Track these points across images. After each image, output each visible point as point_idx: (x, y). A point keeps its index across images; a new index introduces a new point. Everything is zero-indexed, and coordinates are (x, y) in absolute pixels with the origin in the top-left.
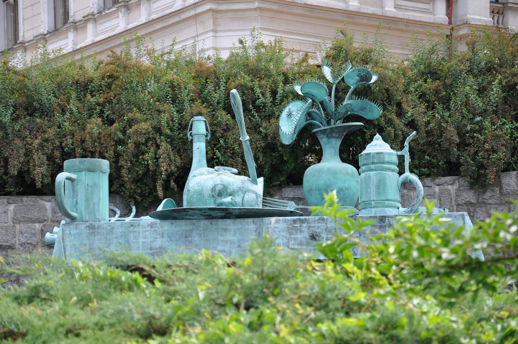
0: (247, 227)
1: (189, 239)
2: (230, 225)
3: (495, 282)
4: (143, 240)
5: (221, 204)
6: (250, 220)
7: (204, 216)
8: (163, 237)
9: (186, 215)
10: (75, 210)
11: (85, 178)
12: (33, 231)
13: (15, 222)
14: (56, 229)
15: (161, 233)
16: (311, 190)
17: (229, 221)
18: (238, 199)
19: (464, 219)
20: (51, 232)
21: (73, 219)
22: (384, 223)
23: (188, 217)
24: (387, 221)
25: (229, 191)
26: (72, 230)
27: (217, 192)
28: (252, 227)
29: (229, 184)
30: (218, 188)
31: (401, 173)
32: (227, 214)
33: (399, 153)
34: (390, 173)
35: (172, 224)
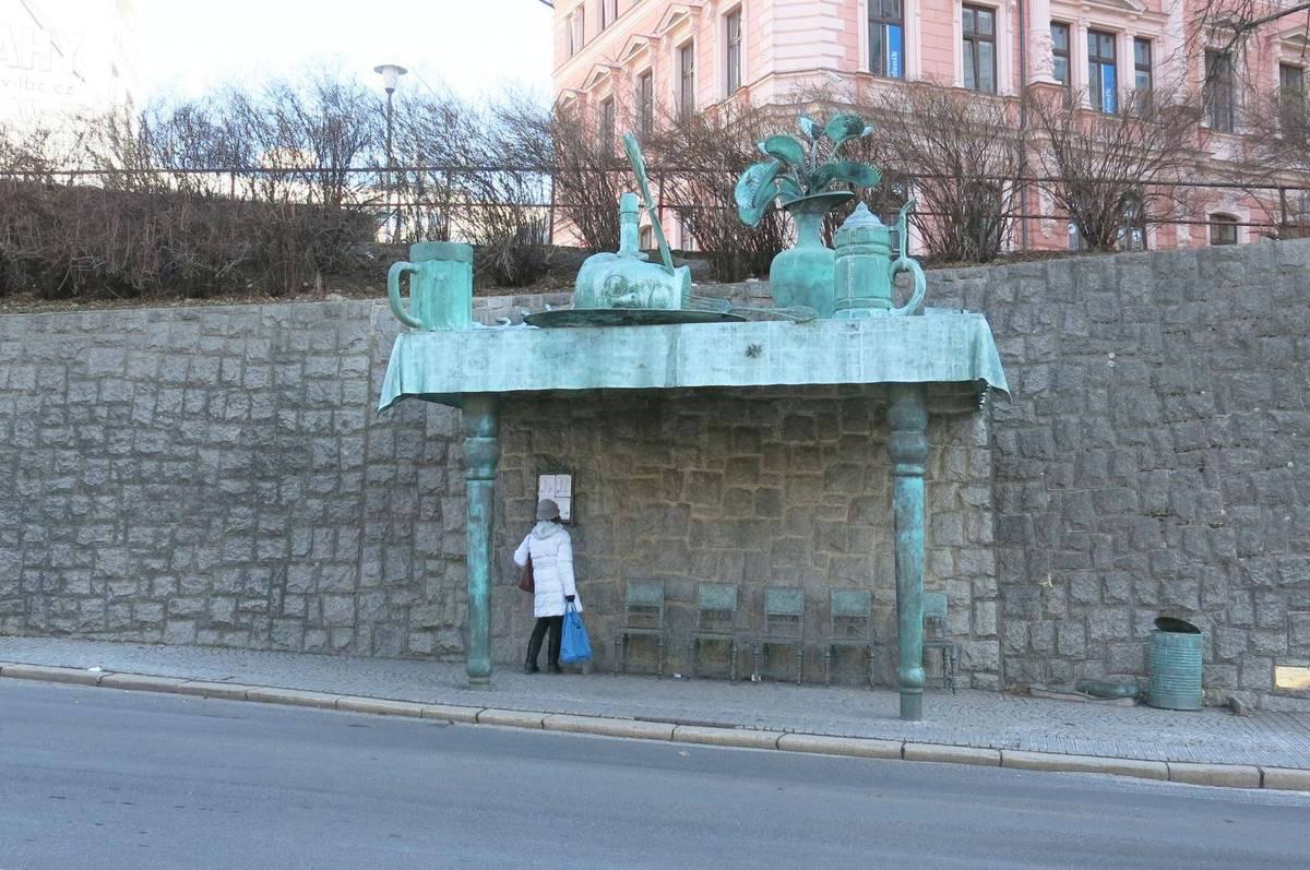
3: (1152, 595)
5: (618, 305)
17: (628, 330)
18: (643, 297)
25: (630, 285)
27: (613, 286)
31: (894, 258)
33: (892, 229)
34: (878, 257)
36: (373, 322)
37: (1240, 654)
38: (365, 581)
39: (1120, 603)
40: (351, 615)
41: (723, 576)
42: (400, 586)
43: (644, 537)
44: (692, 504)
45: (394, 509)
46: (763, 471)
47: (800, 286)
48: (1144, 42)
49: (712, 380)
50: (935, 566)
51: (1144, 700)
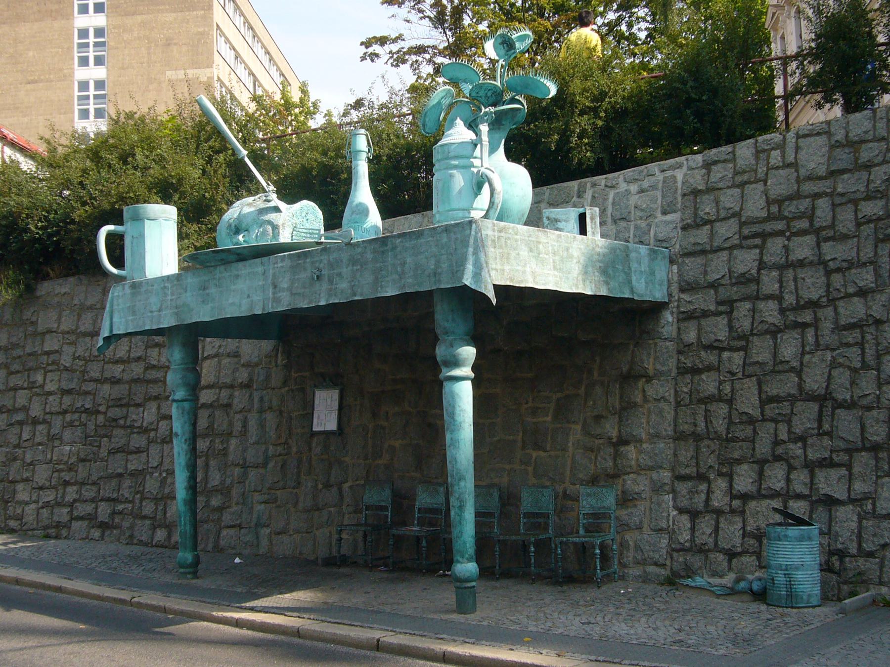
28: (260, 269)
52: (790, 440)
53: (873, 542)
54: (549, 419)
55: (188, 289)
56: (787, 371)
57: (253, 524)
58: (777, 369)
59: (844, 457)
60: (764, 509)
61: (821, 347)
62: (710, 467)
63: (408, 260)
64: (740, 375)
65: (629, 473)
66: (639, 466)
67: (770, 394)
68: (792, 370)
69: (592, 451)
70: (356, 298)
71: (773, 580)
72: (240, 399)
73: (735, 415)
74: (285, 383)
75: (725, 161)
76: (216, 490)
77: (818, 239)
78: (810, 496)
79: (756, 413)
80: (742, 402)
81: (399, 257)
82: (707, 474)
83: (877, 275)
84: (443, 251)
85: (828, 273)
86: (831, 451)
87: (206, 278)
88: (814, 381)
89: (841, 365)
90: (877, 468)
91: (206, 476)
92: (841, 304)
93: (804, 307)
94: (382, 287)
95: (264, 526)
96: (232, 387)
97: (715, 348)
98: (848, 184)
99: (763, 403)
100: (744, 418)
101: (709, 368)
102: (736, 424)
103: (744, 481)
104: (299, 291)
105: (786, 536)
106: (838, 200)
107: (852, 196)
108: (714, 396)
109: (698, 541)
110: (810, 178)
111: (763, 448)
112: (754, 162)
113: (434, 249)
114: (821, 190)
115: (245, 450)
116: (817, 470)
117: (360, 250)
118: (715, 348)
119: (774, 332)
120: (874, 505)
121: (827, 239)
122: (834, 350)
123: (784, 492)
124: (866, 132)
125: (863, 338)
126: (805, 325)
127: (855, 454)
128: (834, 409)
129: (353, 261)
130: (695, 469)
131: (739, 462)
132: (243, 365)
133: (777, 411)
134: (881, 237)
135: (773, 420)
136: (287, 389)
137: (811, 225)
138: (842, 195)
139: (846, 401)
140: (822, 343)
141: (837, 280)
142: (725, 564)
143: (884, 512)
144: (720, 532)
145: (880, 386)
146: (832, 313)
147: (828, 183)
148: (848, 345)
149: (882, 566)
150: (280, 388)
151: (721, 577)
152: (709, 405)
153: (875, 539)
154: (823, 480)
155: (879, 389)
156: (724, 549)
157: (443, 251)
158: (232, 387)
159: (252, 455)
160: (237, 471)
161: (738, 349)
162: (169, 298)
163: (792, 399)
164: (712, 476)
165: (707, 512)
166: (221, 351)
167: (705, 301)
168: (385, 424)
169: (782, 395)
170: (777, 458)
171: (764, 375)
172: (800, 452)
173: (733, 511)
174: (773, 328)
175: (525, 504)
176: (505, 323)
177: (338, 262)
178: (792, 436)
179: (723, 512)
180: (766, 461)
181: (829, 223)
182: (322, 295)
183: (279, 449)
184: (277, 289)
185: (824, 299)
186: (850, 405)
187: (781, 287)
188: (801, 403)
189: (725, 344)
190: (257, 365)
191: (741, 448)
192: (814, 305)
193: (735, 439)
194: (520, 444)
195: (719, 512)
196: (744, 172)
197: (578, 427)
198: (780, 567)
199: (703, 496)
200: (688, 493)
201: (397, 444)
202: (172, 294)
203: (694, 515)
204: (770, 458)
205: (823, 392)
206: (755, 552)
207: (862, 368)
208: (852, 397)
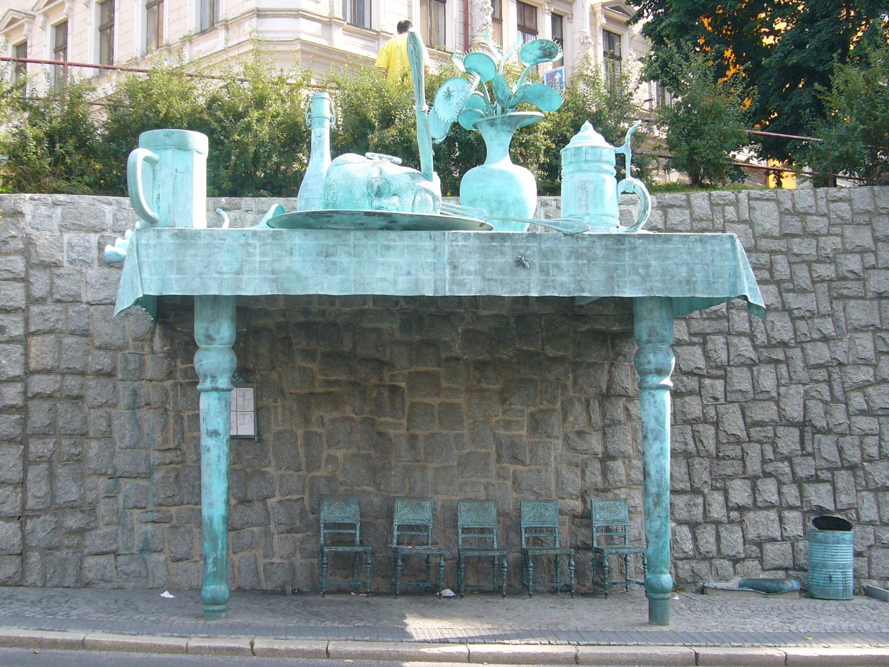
0: (421, 244)
1: (333, 259)
2: (395, 241)
4: (262, 259)
6: (425, 234)
7: (355, 225)
8: (291, 254)
9: (329, 222)
10: (156, 207)
11: (169, 157)
12: (87, 244)
13: (63, 229)
14: (119, 241)
15: (288, 249)
16: (475, 200)
17: (393, 234)
19: (733, 244)
20: (113, 245)
21: (151, 221)
22: (623, 244)
23: (330, 226)
24: (627, 242)
25: (393, 188)
26: (149, 237)
27: (375, 189)
28: (428, 244)
29: (394, 178)
30: (376, 185)
32: (391, 223)
35: (306, 235)
36: (28, 218)
37: (870, 547)
38: (31, 503)
39: (771, 506)
40: (17, 540)
41: (412, 489)
42: (73, 507)
43: (332, 452)
44: (376, 418)
45: (61, 424)
46: (444, 384)
47: (500, 203)
48: (557, 19)
49: (515, 291)
50: (610, 476)
51: (807, 592)
52: (776, 460)
53: (862, 544)
54: (524, 432)
55: (296, 252)
56: (766, 400)
57: (135, 550)
58: (757, 397)
59: (825, 475)
60: (763, 520)
61: (794, 382)
62: (705, 482)
63: (653, 263)
64: (722, 401)
65: (619, 488)
66: (630, 480)
67: (755, 419)
68: (771, 399)
69: (577, 466)
70: (584, 294)
71: (830, 577)
72: (95, 391)
73: (722, 436)
74: (170, 375)
75: (680, 207)
76: (72, 507)
77: (780, 289)
78: (802, 507)
79: (743, 434)
80: (730, 425)
81: (639, 258)
82: (702, 489)
83: (835, 323)
84: (697, 261)
85: (793, 319)
86: (816, 469)
87: (331, 243)
88: (794, 411)
89: (813, 398)
90: (856, 484)
91: (51, 488)
92: (809, 346)
93: (774, 346)
94: (618, 286)
95: (155, 551)
96: (83, 374)
97: (696, 375)
98: (804, 247)
99: (748, 427)
100: (732, 439)
101: (691, 393)
102: (724, 444)
103: (740, 494)
104: (494, 276)
105: (844, 540)
106: (794, 259)
107: (806, 258)
108: (700, 418)
109: (702, 550)
110: (764, 236)
111: (754, 466)
112: (710, 213)
113: (685, 257)
114: (778, 248)
115: (112, 455)
116: (806, 485)
117: (585, 244)
118: (696, 375)
119: (750, 365)
120: (857, 513)
121: (789, 291)
122: (806, 384)
123: (778, 504)
124: (810, 207)
125: (830, 376)
126: (778, 362)
127: (835, 472)
128: (814, 434)
129: (575, 254)
130: (688, 484)
131: (730, 477)
132: (99, 348)
133: (763, 434)
134: (835, 295)
135: (759, 442)
136: (171, 382)
137: (772, 276)
138: (797, 255)
139: (824, 428)
140: (794, 377)
141: (802, 325)
142: (731, 569)
143: (867, 519)
144: (723, 541)
145: (849, 416)
146: (800, 354)
147: (783, 242)
148: (817, 381)
149: (869, 563)
150: (162, 380)
151: (727, 581)
152: (695, 426)
153: (863, 542)
154: (814, 493)
155: (849, 419)
156: (728, 555)
157: (697, 261)
158: (83, 374)
159: (123, 462)
160: (103, 483)
161: (717, 378)
162: (258, 258)
163: (775, 424)
164: (706, 491)
165: (706, 523)
166: (59, 326)
167: (678, 330)
168: (320, 430)
169: (766, 420)
170: (767, 475)
171: (746, 402)
172: (788, 470)
173: (731, 522)
174: (749, 362)
175: (526, 519)
176: (460, 330)
177: (553, 253)
178: (779, 456)
179: (721, 523)
180: (758, 478)
181: (788, 277)
182: (532, 286)
183: (170, 456)
184: (459, 271)
185: (793, 341)
186: (828, 431)
187: (751, 326)
188: (782, 428)
189: (704, 372)
190: (120, 349)
191: (732, 465)
192: (784, 344)
193: (726, 458)
194: (493, 457)
195: (717, 523)
196: (701, 220)
197: (560, 442)
198: (838, 566)
199: (701, 509)
200: (686, 506)
201: (339, 454)
202: (263, 254)
203: (693, 526)
204: (761, 475)
205: (802, 420)
206: (757, 557)
207: (832, 401)
208: (828, 424)
